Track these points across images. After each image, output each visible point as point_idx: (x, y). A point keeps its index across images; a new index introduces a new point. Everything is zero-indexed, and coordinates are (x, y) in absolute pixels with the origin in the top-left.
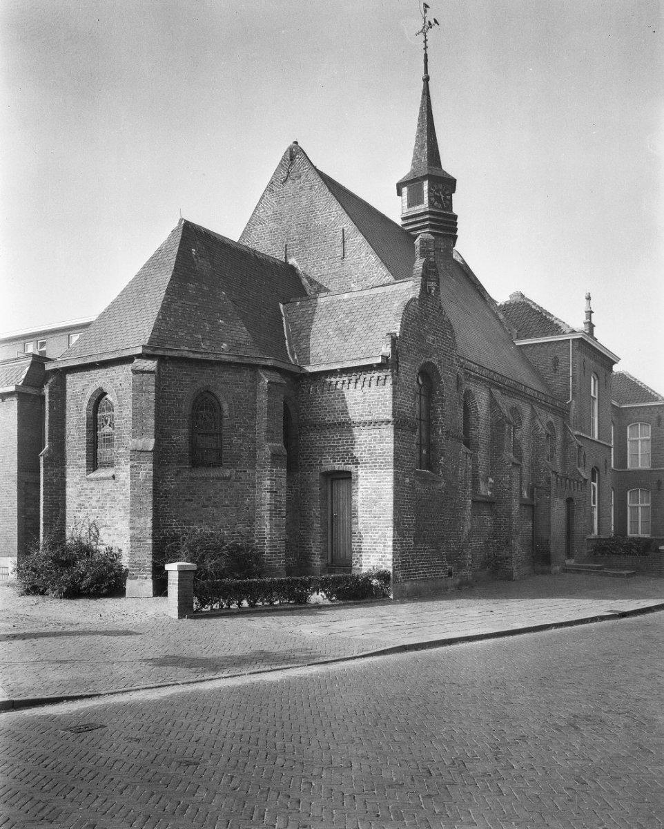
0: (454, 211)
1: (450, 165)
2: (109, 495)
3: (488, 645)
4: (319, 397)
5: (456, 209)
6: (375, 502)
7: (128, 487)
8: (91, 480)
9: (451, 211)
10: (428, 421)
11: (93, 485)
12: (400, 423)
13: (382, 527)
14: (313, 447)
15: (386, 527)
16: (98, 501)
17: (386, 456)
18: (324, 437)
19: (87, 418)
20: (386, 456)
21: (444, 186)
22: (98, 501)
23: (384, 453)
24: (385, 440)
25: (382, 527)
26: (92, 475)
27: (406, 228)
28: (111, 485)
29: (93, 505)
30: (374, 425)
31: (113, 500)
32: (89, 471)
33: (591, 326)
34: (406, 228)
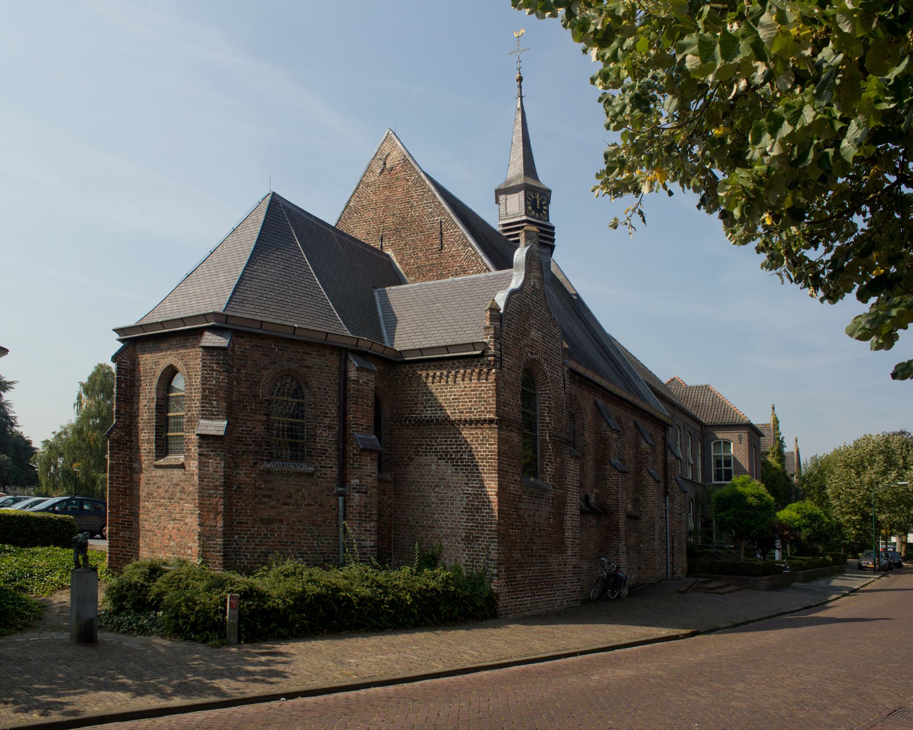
0: (550, 221)
1: (545, 178)
2: (177, 485)
3: (637, 650)
4: (415, 390)
5: (553, 220)
6: (478, 509)
7: (196, 478)
8: (161, 467)
9: (548, 220)
10: (529, 424)
11: (160, 472)
12: (502, 422)
13: (486, 538)
14: (409, 444)
15: (490, 538)
16: (167, 491)
17: (489, 459)
18: (420, 434)
19: (157, 398)
20: (489, 459)
21: (778, 422)
22: (167, 491)
23: (487, 455)
24: (488, 441)
25: (486, 538)
26: (161, 462)
27: (504, 234)
28: (180, 473)
29: (162, 495)
30: (482, 424)
31: (183, 491)
32: (158, 457)
33: (776, 421)
34: (504, 234)
